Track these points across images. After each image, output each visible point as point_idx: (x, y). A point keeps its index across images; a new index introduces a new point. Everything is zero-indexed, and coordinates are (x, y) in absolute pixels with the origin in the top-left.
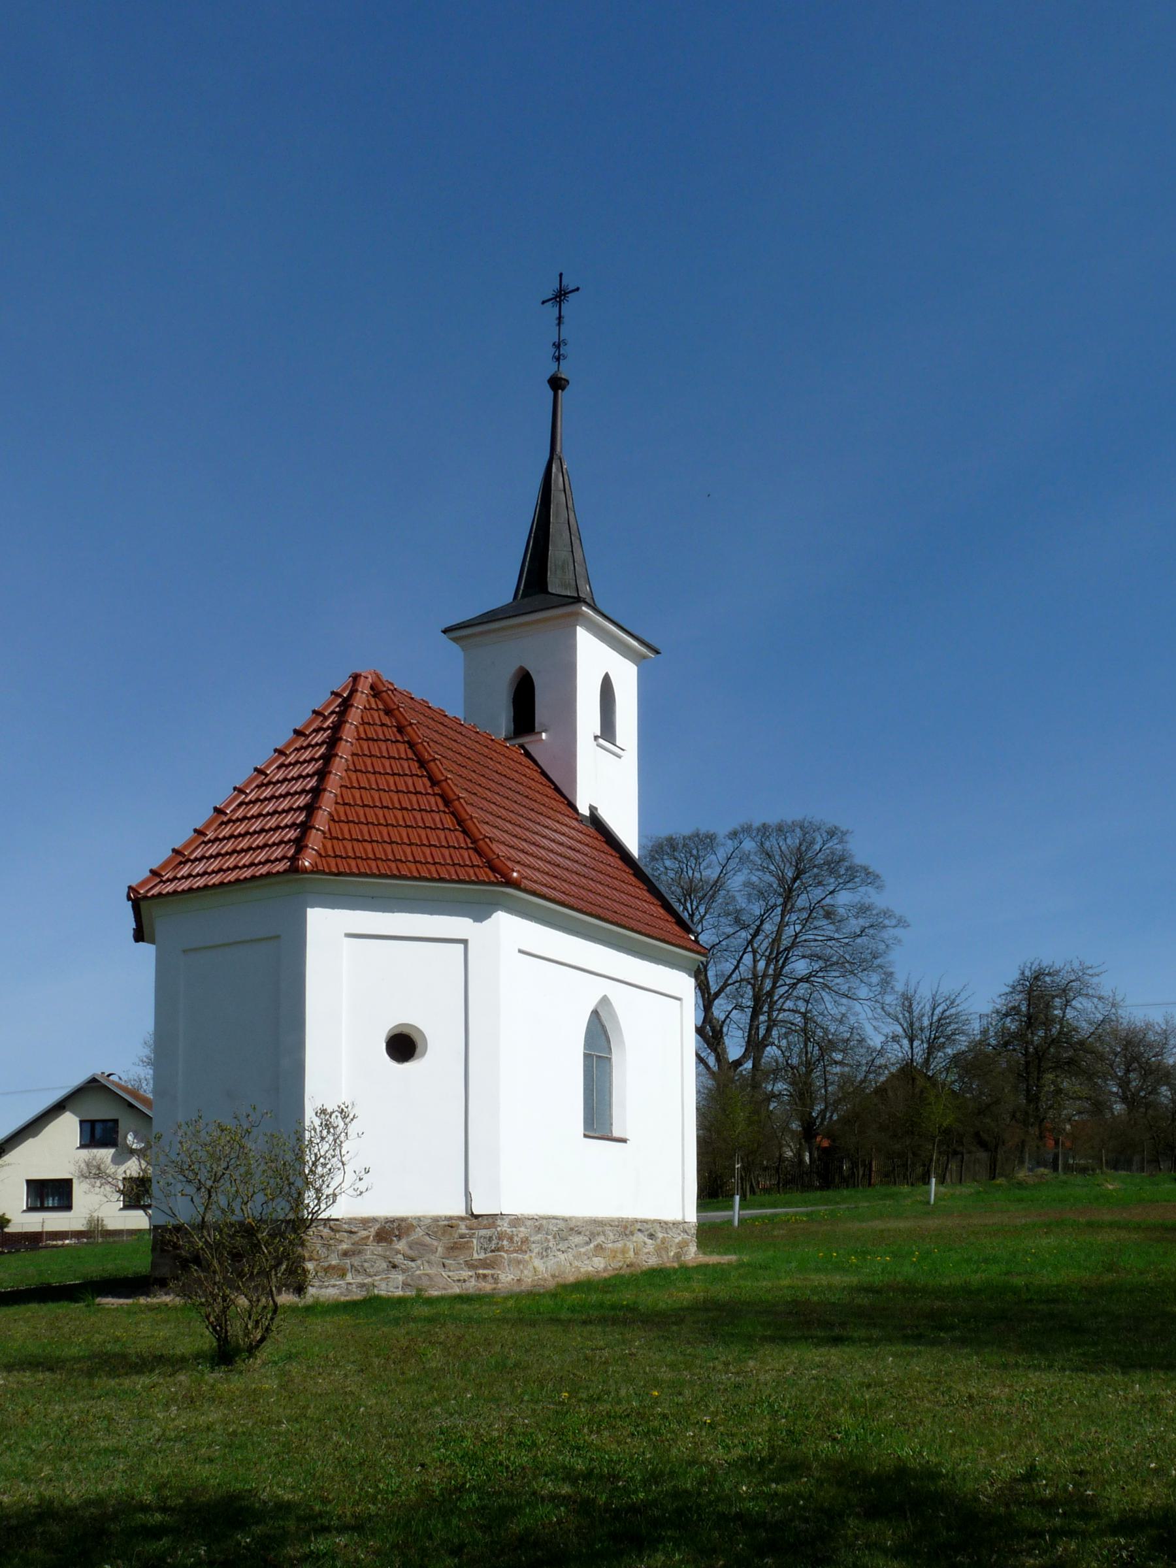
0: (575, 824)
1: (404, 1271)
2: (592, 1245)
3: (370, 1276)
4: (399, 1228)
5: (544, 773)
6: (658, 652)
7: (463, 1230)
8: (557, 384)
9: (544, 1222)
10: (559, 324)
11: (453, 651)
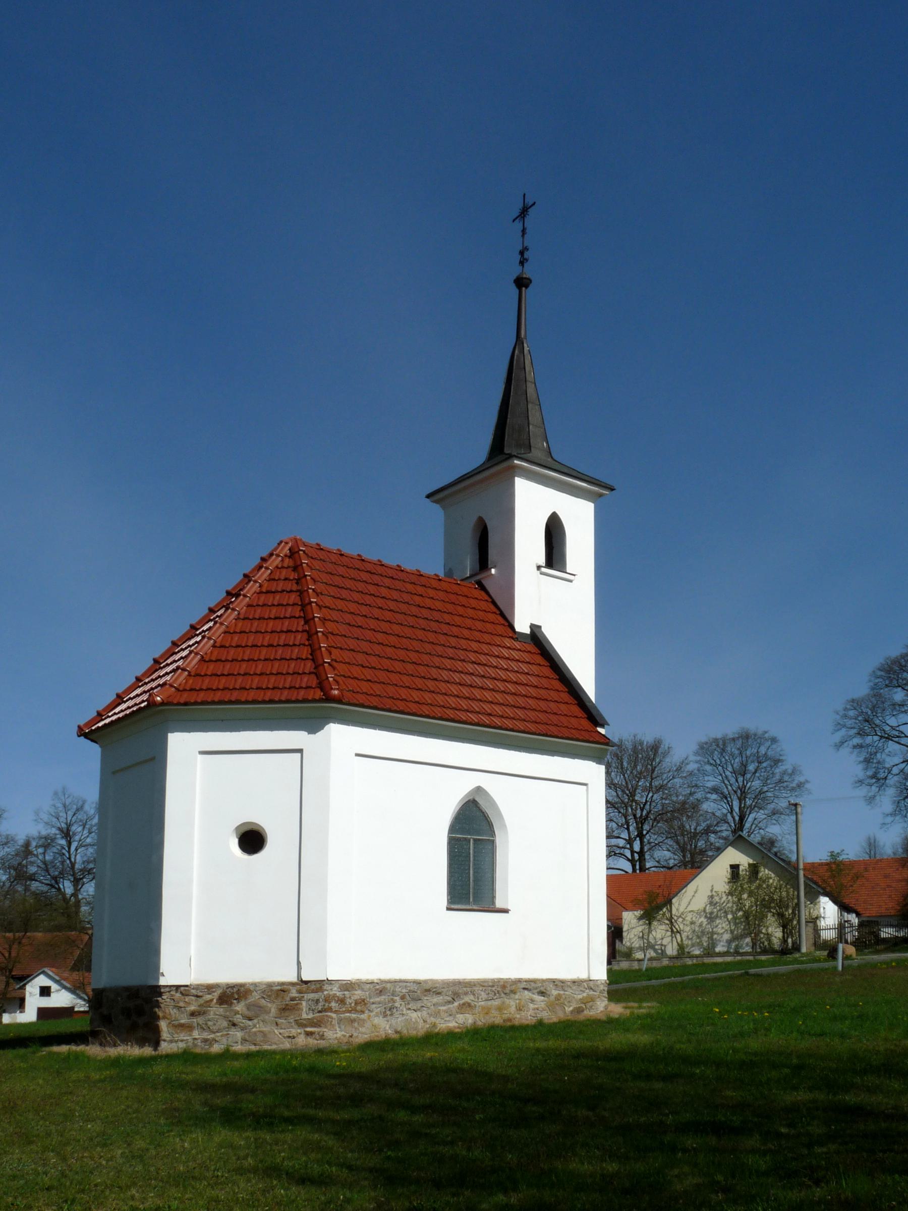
0: (517, 645)
1: (243, 1029)
2: (456, 1004)
3: (214, 1033)
4: (238, 992)
5: (494, 603)
6: (612, 489)
7: (294, 993)
8: (521, 283)
9: (388, 985)
10: (523, 235)
11: (436, 511)
